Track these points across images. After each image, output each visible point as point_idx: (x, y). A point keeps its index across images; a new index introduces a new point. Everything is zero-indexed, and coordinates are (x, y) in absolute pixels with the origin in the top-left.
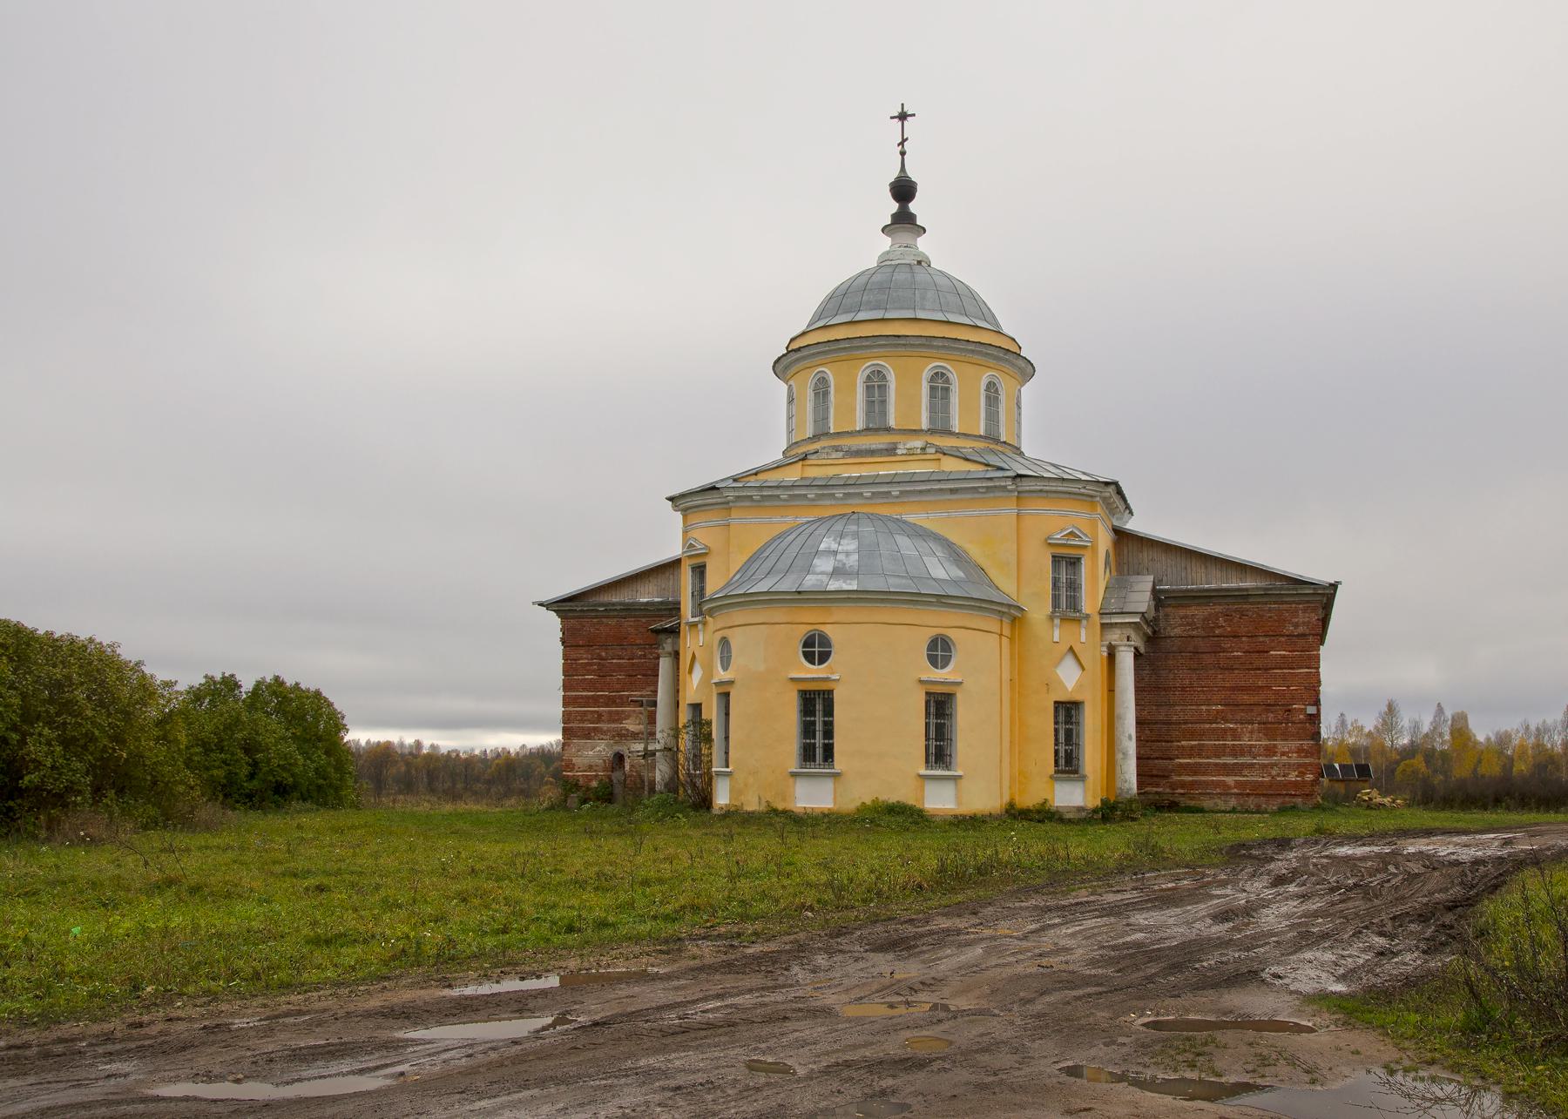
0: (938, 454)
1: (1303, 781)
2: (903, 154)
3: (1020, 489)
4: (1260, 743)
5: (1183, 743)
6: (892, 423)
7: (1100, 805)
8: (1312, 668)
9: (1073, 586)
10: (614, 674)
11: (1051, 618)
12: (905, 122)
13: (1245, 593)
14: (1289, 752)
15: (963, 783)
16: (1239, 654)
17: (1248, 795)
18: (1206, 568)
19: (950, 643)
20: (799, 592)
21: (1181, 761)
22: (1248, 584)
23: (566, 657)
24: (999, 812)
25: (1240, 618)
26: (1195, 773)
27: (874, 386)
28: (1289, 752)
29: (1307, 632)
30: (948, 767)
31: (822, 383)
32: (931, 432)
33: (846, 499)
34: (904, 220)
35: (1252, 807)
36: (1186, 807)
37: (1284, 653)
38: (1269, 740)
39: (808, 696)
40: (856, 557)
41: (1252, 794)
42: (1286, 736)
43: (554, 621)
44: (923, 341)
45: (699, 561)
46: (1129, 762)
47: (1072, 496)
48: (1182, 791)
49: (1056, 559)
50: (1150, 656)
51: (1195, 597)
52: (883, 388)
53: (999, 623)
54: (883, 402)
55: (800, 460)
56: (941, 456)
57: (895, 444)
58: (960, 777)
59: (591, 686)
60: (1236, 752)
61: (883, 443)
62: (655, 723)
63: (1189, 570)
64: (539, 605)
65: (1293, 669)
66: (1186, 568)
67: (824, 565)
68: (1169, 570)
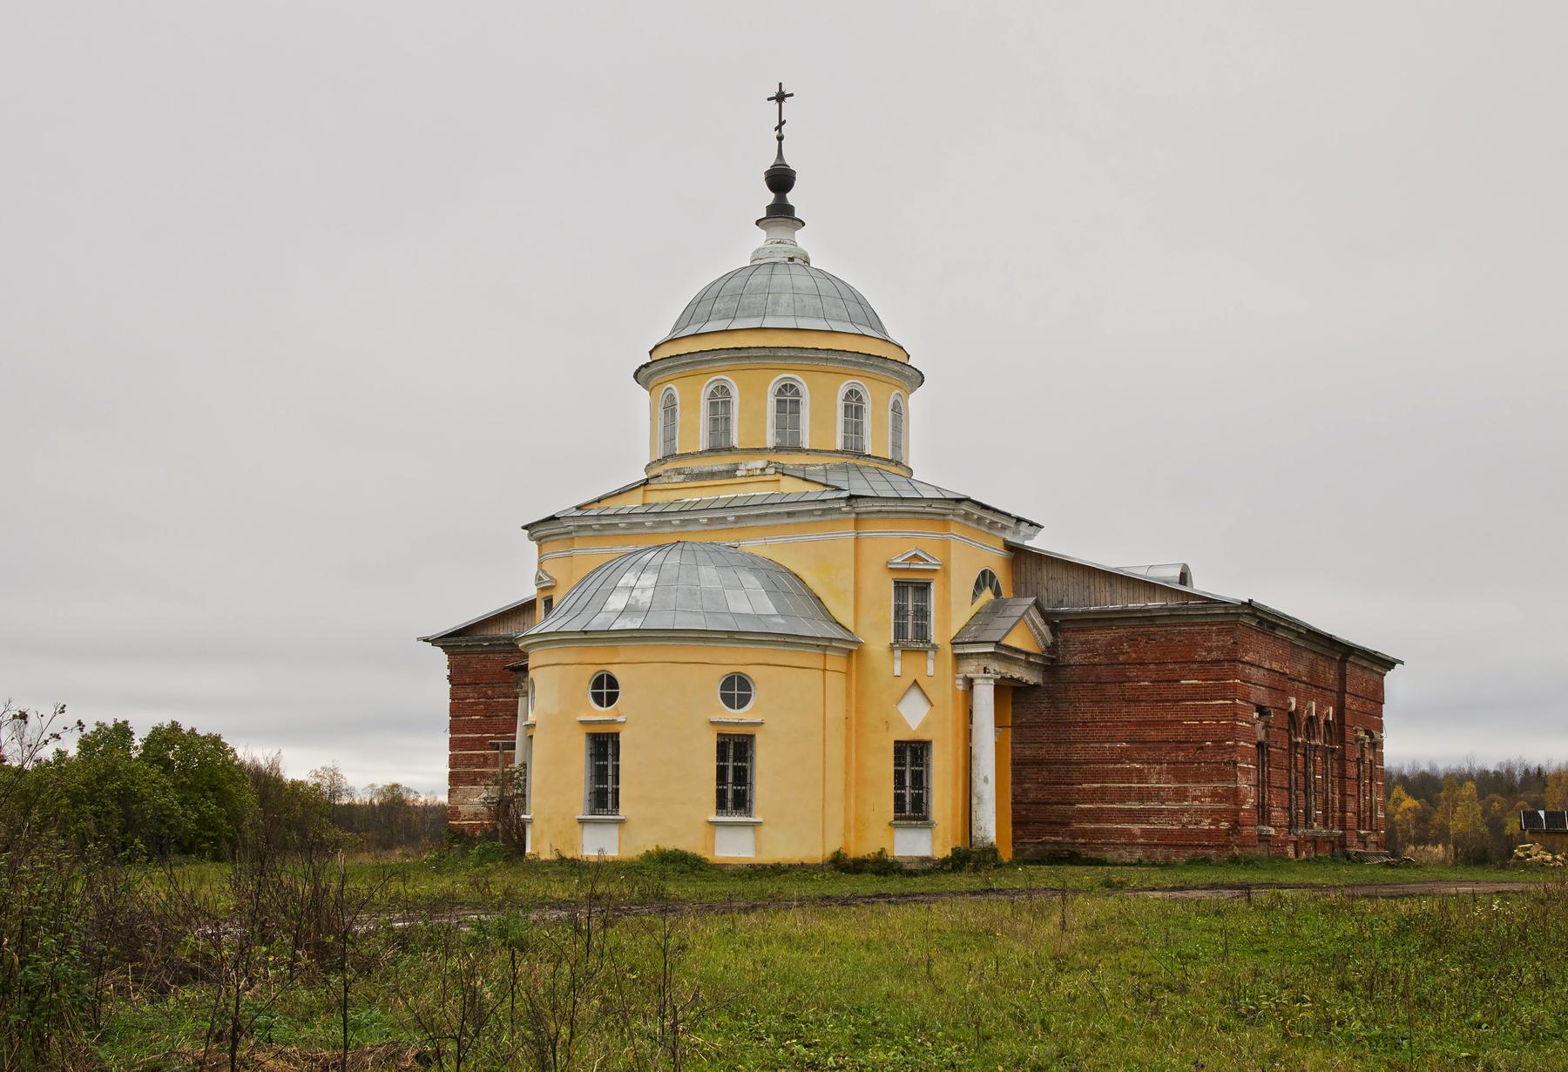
0: (777, 474)
1: (1217, 830)
2: (780, 139)
3: (858, 510)
4: (1169, 785)
5: (1084, 785)
6: (735, 442)
7: (950, 855)
8: (1227, 699)
9: (922, 613)
10: (500, 714)
11: (892, 648)
12: (783, 104)
13: (1148, 615)
14: (1201, 797)
15: (764, 829)
16: (1147, 683)
17: (1156, 845)
18: (1111, 586)
19: (750, 682)
20: (586, 632)
21: (1082, 806)
22: (1156, 603)
23: (453, 697)
24: (820, 861)
25: (1146, 643)
26: (1098, 821)
27: (786, 401)
28: (1201, 797)
29: (1222, 657)
30: (748, 812)
31: (670, 408)
32: (778, 449)
33: (657, 528)
34: (780, 212)
35: (1160, 859)
36: (1088, 859)
37: (1196, 681)
38: (1179, 783)
39: (597, 739)
40: (651, 592)
41: (1161, 845)
42: (1198, 778)
43: (440, 658)
44: (766, 352)
45: (547, 594)
46: (984, 807)
47: (917, 516)
48: (1083, 841)
49: (900, 587)
50: (1048, 687)
51: (1095, 620)
52: (727, 404)
53: (822, 658)
54: (727, 419)
55: (641, 485)
56: (779, 476)
57: (736, 464)
58: (759, 823)
59: (478, 727)
60: (1144, 795)
61: (725, 465)
62: (1015, 763)
63: (1092, 587)
64: (424, 641)
65: (1207, 700)
66: (1089, 587)
67: (617, 602)
68: (1071, 590)
